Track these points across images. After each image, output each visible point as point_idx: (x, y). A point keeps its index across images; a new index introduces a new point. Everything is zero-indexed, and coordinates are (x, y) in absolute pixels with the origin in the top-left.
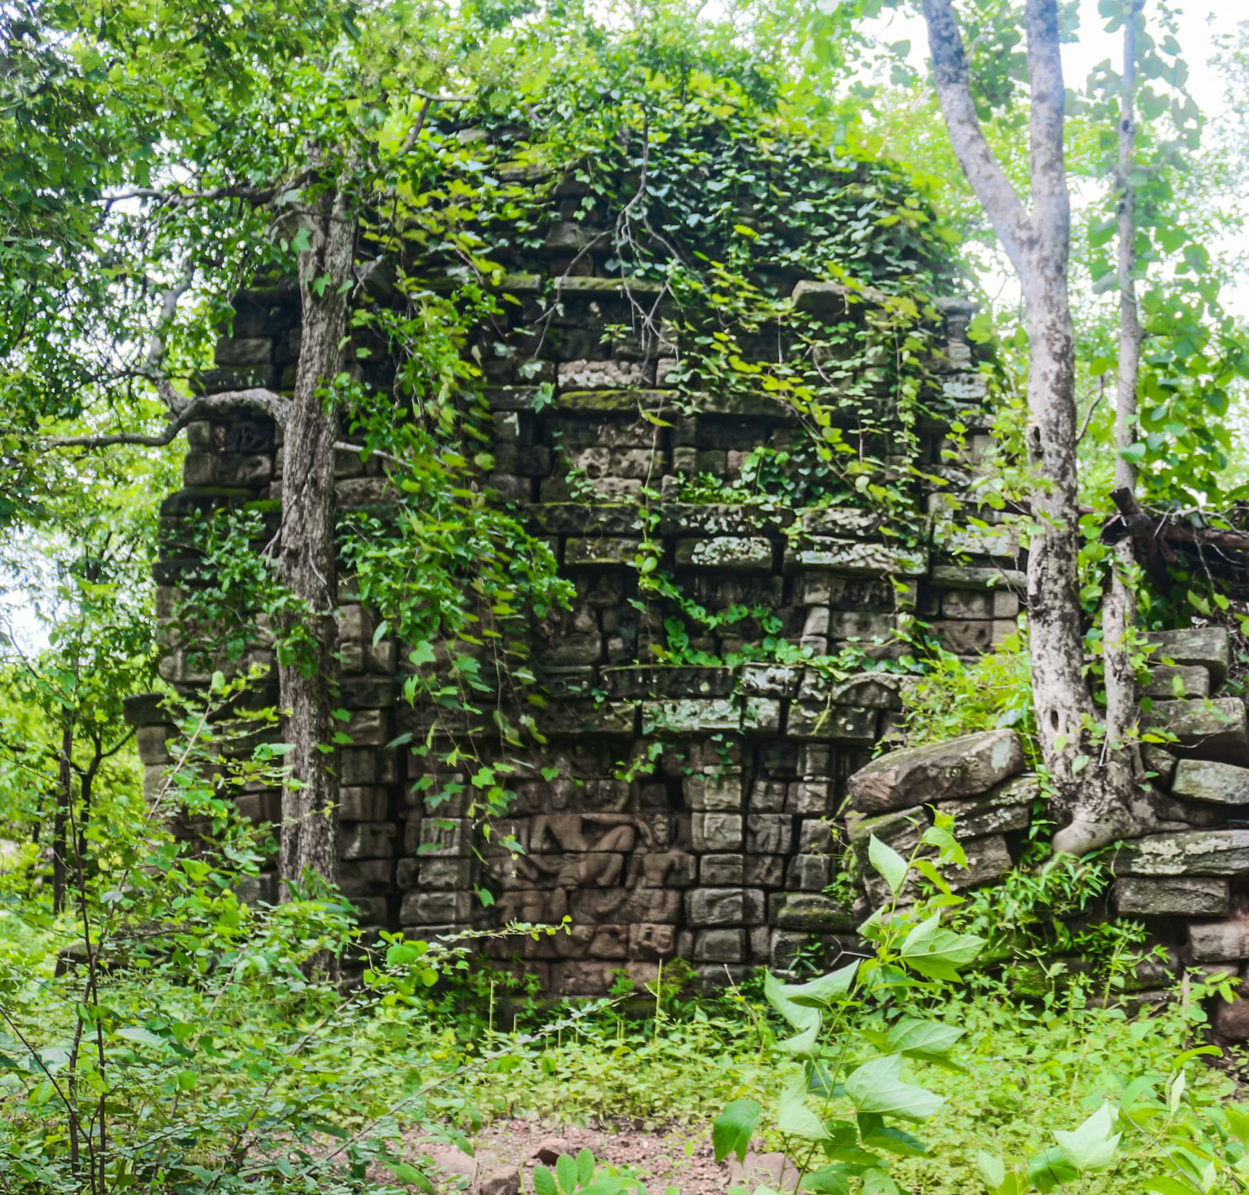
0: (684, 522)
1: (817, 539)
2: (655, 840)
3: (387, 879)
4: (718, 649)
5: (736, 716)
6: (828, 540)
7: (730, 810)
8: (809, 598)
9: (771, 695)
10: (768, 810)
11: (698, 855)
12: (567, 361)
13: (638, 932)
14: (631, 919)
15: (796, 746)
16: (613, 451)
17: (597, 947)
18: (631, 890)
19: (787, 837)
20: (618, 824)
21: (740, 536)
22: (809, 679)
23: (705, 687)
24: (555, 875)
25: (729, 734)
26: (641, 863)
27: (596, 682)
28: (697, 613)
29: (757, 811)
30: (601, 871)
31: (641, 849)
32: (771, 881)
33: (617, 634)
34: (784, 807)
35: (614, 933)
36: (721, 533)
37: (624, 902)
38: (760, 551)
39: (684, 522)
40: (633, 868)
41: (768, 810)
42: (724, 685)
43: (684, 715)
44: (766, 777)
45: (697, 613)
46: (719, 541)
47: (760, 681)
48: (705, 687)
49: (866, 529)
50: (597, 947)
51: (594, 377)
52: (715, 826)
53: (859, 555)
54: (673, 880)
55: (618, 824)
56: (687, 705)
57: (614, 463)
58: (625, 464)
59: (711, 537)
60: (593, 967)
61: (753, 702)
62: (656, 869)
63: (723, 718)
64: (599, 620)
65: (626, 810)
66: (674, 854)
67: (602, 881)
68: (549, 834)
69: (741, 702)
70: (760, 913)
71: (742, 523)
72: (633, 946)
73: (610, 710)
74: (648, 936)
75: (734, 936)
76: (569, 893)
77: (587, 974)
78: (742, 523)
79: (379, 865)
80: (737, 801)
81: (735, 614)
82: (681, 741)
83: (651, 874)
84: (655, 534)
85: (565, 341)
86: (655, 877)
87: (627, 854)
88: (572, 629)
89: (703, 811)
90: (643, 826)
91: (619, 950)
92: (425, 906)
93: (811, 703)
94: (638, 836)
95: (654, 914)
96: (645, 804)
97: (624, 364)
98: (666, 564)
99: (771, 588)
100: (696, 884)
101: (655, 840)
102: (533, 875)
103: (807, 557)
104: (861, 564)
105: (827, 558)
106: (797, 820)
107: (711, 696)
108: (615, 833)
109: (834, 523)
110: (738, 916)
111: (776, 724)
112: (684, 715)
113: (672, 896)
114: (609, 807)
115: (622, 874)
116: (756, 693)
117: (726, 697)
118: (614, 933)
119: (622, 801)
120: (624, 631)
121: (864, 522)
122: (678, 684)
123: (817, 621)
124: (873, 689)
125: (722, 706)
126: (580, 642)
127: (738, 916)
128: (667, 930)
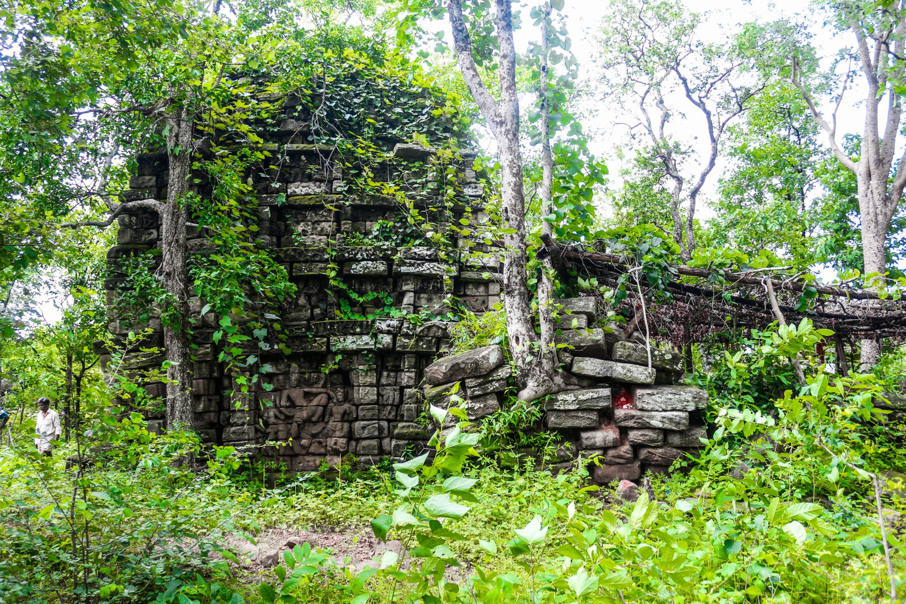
0: (347, 255)
1: (408, 261)
2: (338, 400)
3: (216, 421)
4: (364, 313)
5: (372, 342)
6: (413, 261)
7: (371, 385)
8: (405, 288)
9: (389, 332)
10: (389, 385)
11: (357, 406)
12: (292, 182)
13: (331, 442)
14: (328, 436)
15: (400, 356)
16: (313, 223)
17: (312, 449)
18: (327, 423)
19: (397, 397)
20: (320, 393)
21: (373, 260)
22: (406, 325)
23: (358, 330)
24: (292, 417)
25: (370, 351)
26: (331, 411)
27: (309, 328)
28: (354, 296)
29: (383, 385)
30: (313, 415)
31: (331, 404)
32: (391, 417)
33: (318, 307)
34: (396, 384)
35: (320, 443)
36: (363, 259)
37: (324, 428)
38: (381, 267)
39: (347, 255)
40: (328, 412)
41: (389, 385)
42: (368, 329)
43: (350, 343)
44: (387, 370)
45: (354, 296)
46: (363, 263)
47: (384, 326)
48: (358, 330)
49: (430, 256)
50: (312, 449)
51: (304, 189)
52: (365, 393)
53: (427, 268)
54: (346, 418)
55: (320, 393)
56: (350, 339)
57: (314, 229)
58: (319, 229)
59: (359, 261)
60: (311, 458)
61: (380, 336)
62: (338, 413)
63: (367, 344)
64: (309, 301)
65: (324, 386)
66: (346, 406)
67: (314, 419)
68: (289, 398)
69: (375, 336)
70: (386, 432)
71: (373, 254)
72: (329, 448)
73: (315, 341)
74: (336, 444)
75: (374, 442)
76: (299, 425)
77: (308, 461)
78: (373, 254)
79: (212, 414)
80: (374, 381)
81: (371, 296)
82: (349, 354)
83: (336, 416)
84: (334, 261)
85: (290, 174)
86: (338, 417)
87: (325, 407)
88: (297, 305)
89: (359, 386)
90: (331, 393)
91: (323, 450)
92: (234, 433)
93: (407, 336)
94: (330, 398)
95: (338, 433)
96: (332, 384)
97: (318, 183)
98: (340, 274)
99: (387, 284)
100: (357, 419)
101: (338, 400)
102: (282, 417)
103: (404, 269)
104: (428, 272)
105: (412, 270)
106: (402, 389)
107: (361, 334)
108: (319, 397)
109: (415, 253)
110: (376, 433)
111: (391, 346)
112: (350, 343)
113: (346, 425)
114: (316, 386)
115: (323, 416)
116: (382, 332)
117: (368, 334)
118: (320, 443)
119: (322, 382)
120: (321, 305)
121: (429, 253)
122: (347, 329)
123: (408, 299)
124: (435, 329)
125: (366, 338)
126: (301, 311)
127: (376, 433)
128: (344, 441)
